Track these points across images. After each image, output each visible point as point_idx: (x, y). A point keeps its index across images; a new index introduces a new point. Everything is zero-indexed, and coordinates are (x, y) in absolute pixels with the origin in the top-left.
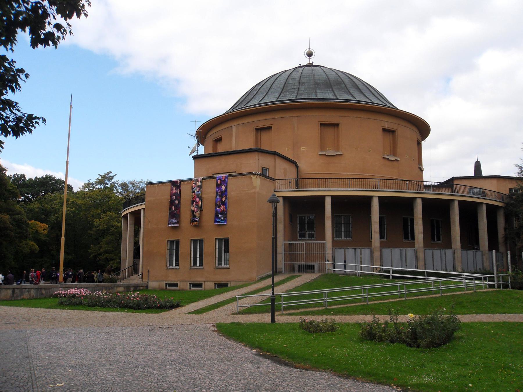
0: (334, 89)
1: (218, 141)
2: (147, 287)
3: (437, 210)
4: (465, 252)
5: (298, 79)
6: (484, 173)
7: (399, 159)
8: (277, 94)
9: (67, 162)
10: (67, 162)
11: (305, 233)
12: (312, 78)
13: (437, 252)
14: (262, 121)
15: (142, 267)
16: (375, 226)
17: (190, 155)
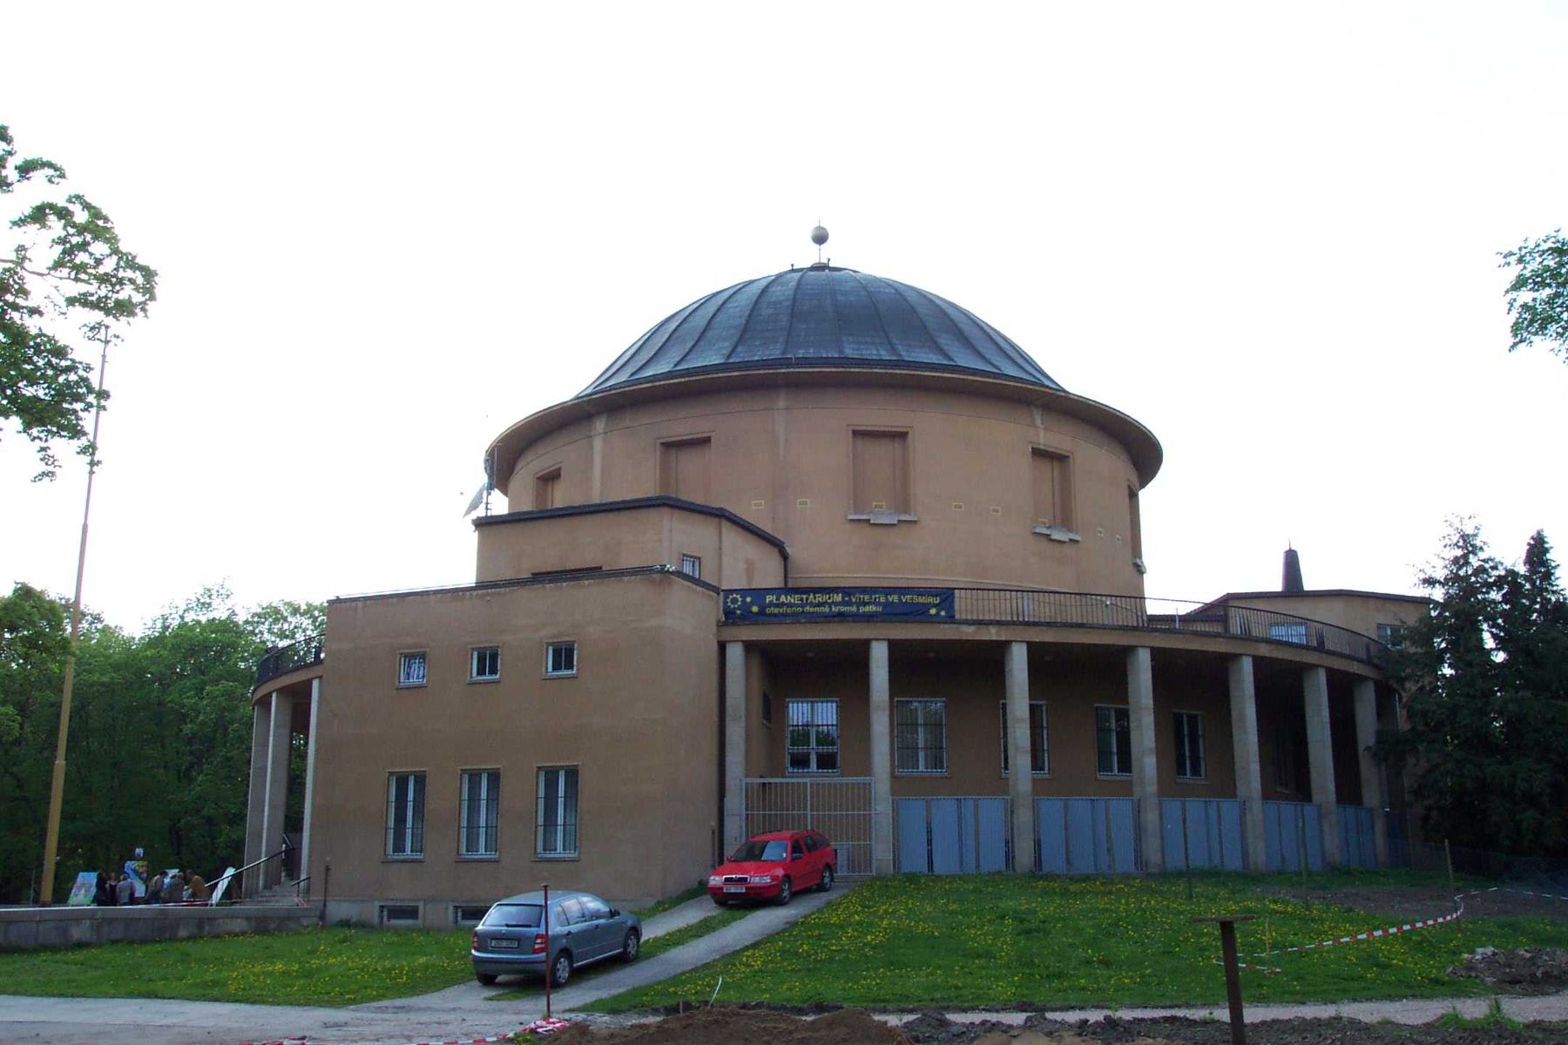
13: (1194, 806)
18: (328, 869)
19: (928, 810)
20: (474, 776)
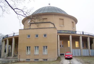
13: (85, 50)
18: (20, 56)
19: (75, 50)
20: (36, 47)
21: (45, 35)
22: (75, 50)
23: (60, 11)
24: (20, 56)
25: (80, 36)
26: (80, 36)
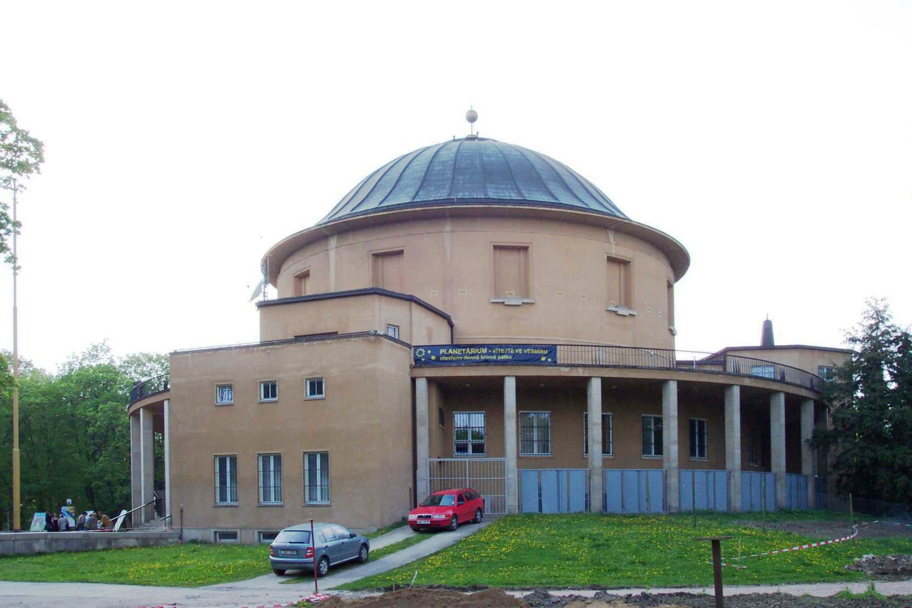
0: (518, 183)
1: (303, 276)
2: (181, 538)
3: (703, 396)
4: (747, 474)
5: (452, 162)
6: (777, 342)
7: (634, 313)
8: (412, 190)
9: (15, 309)
10: (15, 309)
11: (467, 445)
12: (478, 162)
13: (700, 474)
14: (386, 240)
15: (171, 503)
16: (596, 432)
17: (252, 299)
18: (182, 511)
19: (539, 477)
20: (266, 458)
21: (316, 386)
22: (539, 477)
23: (577, 198)
24: (185, 513)
25: (665, 382)
26: (665, 382)
